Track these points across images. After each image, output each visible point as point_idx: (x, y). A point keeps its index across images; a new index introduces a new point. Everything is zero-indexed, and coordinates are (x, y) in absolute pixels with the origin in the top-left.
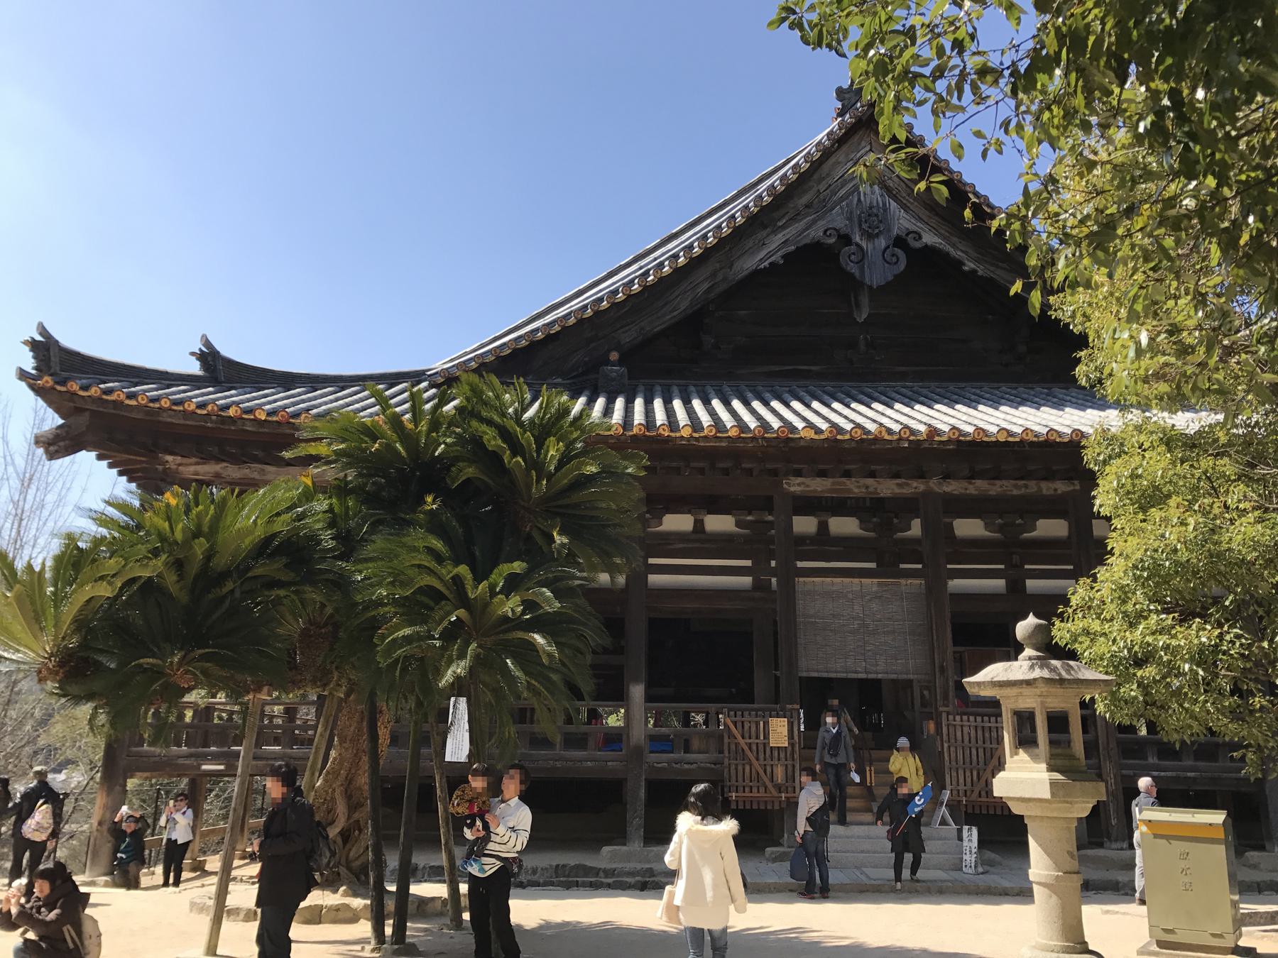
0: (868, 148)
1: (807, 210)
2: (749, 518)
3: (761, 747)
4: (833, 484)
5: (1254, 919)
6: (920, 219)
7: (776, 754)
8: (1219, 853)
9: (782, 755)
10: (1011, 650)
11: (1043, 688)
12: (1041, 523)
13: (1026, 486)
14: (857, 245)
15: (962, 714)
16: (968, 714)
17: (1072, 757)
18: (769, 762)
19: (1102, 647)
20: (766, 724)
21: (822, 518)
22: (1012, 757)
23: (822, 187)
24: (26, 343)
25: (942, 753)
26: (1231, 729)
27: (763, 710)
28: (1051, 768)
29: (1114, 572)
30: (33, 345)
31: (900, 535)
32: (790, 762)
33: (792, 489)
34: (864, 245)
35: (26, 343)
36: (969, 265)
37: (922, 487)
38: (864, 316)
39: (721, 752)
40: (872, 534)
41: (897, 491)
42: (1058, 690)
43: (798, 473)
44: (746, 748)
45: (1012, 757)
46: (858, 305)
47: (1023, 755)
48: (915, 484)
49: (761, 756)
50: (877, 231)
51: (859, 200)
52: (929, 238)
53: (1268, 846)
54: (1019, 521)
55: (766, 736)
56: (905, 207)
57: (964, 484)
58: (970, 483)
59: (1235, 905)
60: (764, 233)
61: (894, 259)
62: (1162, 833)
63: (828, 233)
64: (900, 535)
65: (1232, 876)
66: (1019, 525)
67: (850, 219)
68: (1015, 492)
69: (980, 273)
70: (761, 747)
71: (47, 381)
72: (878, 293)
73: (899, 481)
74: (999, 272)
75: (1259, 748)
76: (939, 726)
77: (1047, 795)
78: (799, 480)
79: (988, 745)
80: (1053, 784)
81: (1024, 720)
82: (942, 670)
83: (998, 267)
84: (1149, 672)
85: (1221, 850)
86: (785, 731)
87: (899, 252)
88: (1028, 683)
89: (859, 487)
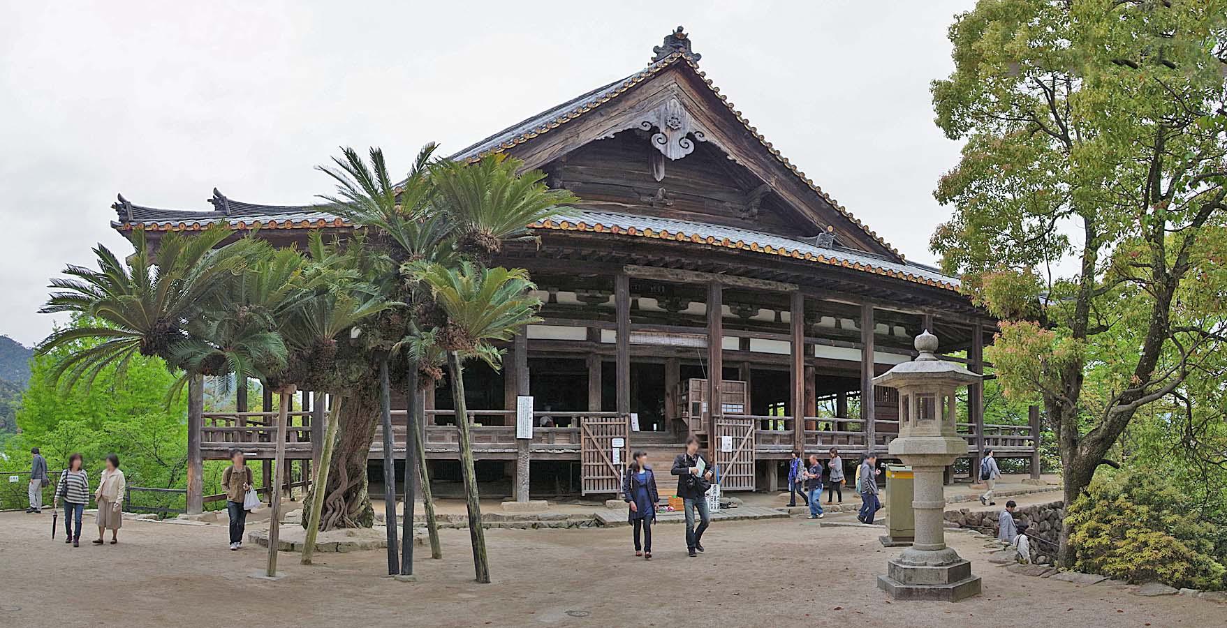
0: (674, 81)
1: (631, 110)
2: (586, 295)
12: (761, 311)
21: (636, 298)
23: (642, 98)
24: (113, 207)
30: (116, 206)
31: (682, 311)
33: (629, 273)
35: (113, 207)
38: (662, 177)
40: (665, 310)
43: (634, 262)
46: (658, 171)
48: (707, 276)
50: (677, 127)
51: (666, 109)
52: (709, 137)
58: (739, 278)
60: (603, 119)
61: (686, 146)
63: (644, 124)
64: (682, 311)
67: (659, 118)
69: (737, 162)
71: (128, 226)
73: (697, 273)
89: (672, 275)
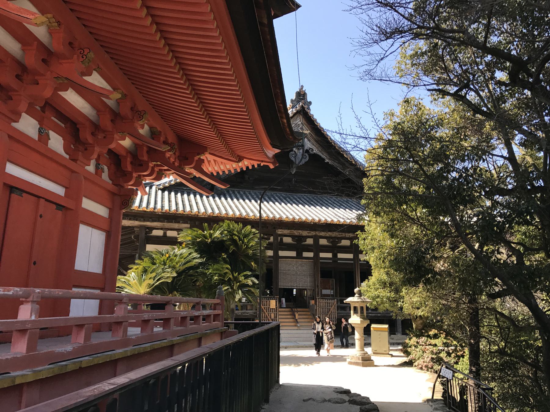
3: (268, 308)
4: (290, 232)
5: (392, 350)
6: (313, 144)
7: (272, 310)
8: (386, 334)
9: (273, 311)
10: (353, 295)
11: (360, 303)
13: (342, 234)
14: (294, 151)
15: (322, 299)
16: (324, 299)
17: (364, 316)
18: (270, 313)
19: (370, 294)
20: (269, 302)
22: (353, 315)
25: (316, 310)
26: (391, 309)
27: (269, 298)
28: (360, 318)
29: (373, 279)
32: (276, 313)
33: (279, 233)
34: (296, 151)
36: (327, 161)
37: (314, 234)
39: (257, 310)
40: (295, 243)
41: (307, 234)
42: (363, 303)
44: (264, 309)
45: (353, 315)
47: (355, 315)
49: (268, 311)
52: (316, 151)
53: (396, 333)
54: (337, 240)
55: (269, 305)
56: (309, 140)
57: (326, 233)
59: (389, 348)
62: (376, 330)
65: (389, 341)
66: (337, 241)
68: (339, 236)
70: (268, 308)
72: (298, 167)
74: (335, 163)
75: (396, 313)
76: (316, 303)
77: (360, 323)
78: (281, 230)
79: (329, 307)
80: (361, 321)
81: (355, 308)
82: (318, 286)
83: (335, 162)
84: (378, 300)
85: (387, 333)
86: (275, 304)
87: (306, 154)
88: (358, 302)
